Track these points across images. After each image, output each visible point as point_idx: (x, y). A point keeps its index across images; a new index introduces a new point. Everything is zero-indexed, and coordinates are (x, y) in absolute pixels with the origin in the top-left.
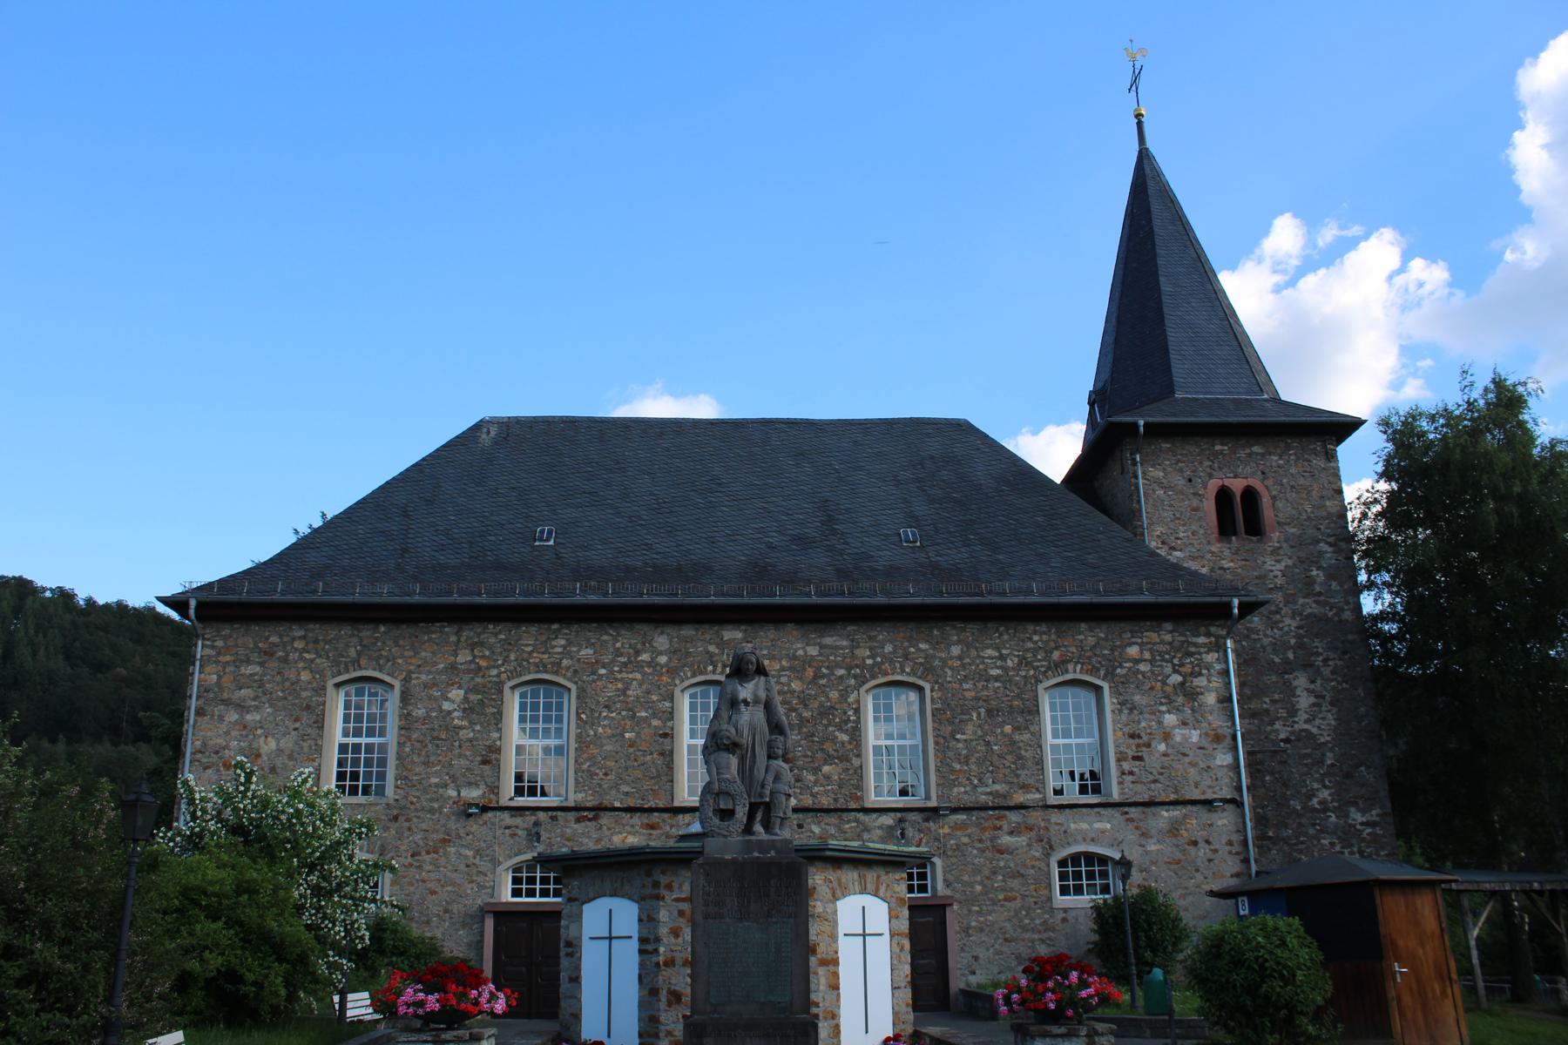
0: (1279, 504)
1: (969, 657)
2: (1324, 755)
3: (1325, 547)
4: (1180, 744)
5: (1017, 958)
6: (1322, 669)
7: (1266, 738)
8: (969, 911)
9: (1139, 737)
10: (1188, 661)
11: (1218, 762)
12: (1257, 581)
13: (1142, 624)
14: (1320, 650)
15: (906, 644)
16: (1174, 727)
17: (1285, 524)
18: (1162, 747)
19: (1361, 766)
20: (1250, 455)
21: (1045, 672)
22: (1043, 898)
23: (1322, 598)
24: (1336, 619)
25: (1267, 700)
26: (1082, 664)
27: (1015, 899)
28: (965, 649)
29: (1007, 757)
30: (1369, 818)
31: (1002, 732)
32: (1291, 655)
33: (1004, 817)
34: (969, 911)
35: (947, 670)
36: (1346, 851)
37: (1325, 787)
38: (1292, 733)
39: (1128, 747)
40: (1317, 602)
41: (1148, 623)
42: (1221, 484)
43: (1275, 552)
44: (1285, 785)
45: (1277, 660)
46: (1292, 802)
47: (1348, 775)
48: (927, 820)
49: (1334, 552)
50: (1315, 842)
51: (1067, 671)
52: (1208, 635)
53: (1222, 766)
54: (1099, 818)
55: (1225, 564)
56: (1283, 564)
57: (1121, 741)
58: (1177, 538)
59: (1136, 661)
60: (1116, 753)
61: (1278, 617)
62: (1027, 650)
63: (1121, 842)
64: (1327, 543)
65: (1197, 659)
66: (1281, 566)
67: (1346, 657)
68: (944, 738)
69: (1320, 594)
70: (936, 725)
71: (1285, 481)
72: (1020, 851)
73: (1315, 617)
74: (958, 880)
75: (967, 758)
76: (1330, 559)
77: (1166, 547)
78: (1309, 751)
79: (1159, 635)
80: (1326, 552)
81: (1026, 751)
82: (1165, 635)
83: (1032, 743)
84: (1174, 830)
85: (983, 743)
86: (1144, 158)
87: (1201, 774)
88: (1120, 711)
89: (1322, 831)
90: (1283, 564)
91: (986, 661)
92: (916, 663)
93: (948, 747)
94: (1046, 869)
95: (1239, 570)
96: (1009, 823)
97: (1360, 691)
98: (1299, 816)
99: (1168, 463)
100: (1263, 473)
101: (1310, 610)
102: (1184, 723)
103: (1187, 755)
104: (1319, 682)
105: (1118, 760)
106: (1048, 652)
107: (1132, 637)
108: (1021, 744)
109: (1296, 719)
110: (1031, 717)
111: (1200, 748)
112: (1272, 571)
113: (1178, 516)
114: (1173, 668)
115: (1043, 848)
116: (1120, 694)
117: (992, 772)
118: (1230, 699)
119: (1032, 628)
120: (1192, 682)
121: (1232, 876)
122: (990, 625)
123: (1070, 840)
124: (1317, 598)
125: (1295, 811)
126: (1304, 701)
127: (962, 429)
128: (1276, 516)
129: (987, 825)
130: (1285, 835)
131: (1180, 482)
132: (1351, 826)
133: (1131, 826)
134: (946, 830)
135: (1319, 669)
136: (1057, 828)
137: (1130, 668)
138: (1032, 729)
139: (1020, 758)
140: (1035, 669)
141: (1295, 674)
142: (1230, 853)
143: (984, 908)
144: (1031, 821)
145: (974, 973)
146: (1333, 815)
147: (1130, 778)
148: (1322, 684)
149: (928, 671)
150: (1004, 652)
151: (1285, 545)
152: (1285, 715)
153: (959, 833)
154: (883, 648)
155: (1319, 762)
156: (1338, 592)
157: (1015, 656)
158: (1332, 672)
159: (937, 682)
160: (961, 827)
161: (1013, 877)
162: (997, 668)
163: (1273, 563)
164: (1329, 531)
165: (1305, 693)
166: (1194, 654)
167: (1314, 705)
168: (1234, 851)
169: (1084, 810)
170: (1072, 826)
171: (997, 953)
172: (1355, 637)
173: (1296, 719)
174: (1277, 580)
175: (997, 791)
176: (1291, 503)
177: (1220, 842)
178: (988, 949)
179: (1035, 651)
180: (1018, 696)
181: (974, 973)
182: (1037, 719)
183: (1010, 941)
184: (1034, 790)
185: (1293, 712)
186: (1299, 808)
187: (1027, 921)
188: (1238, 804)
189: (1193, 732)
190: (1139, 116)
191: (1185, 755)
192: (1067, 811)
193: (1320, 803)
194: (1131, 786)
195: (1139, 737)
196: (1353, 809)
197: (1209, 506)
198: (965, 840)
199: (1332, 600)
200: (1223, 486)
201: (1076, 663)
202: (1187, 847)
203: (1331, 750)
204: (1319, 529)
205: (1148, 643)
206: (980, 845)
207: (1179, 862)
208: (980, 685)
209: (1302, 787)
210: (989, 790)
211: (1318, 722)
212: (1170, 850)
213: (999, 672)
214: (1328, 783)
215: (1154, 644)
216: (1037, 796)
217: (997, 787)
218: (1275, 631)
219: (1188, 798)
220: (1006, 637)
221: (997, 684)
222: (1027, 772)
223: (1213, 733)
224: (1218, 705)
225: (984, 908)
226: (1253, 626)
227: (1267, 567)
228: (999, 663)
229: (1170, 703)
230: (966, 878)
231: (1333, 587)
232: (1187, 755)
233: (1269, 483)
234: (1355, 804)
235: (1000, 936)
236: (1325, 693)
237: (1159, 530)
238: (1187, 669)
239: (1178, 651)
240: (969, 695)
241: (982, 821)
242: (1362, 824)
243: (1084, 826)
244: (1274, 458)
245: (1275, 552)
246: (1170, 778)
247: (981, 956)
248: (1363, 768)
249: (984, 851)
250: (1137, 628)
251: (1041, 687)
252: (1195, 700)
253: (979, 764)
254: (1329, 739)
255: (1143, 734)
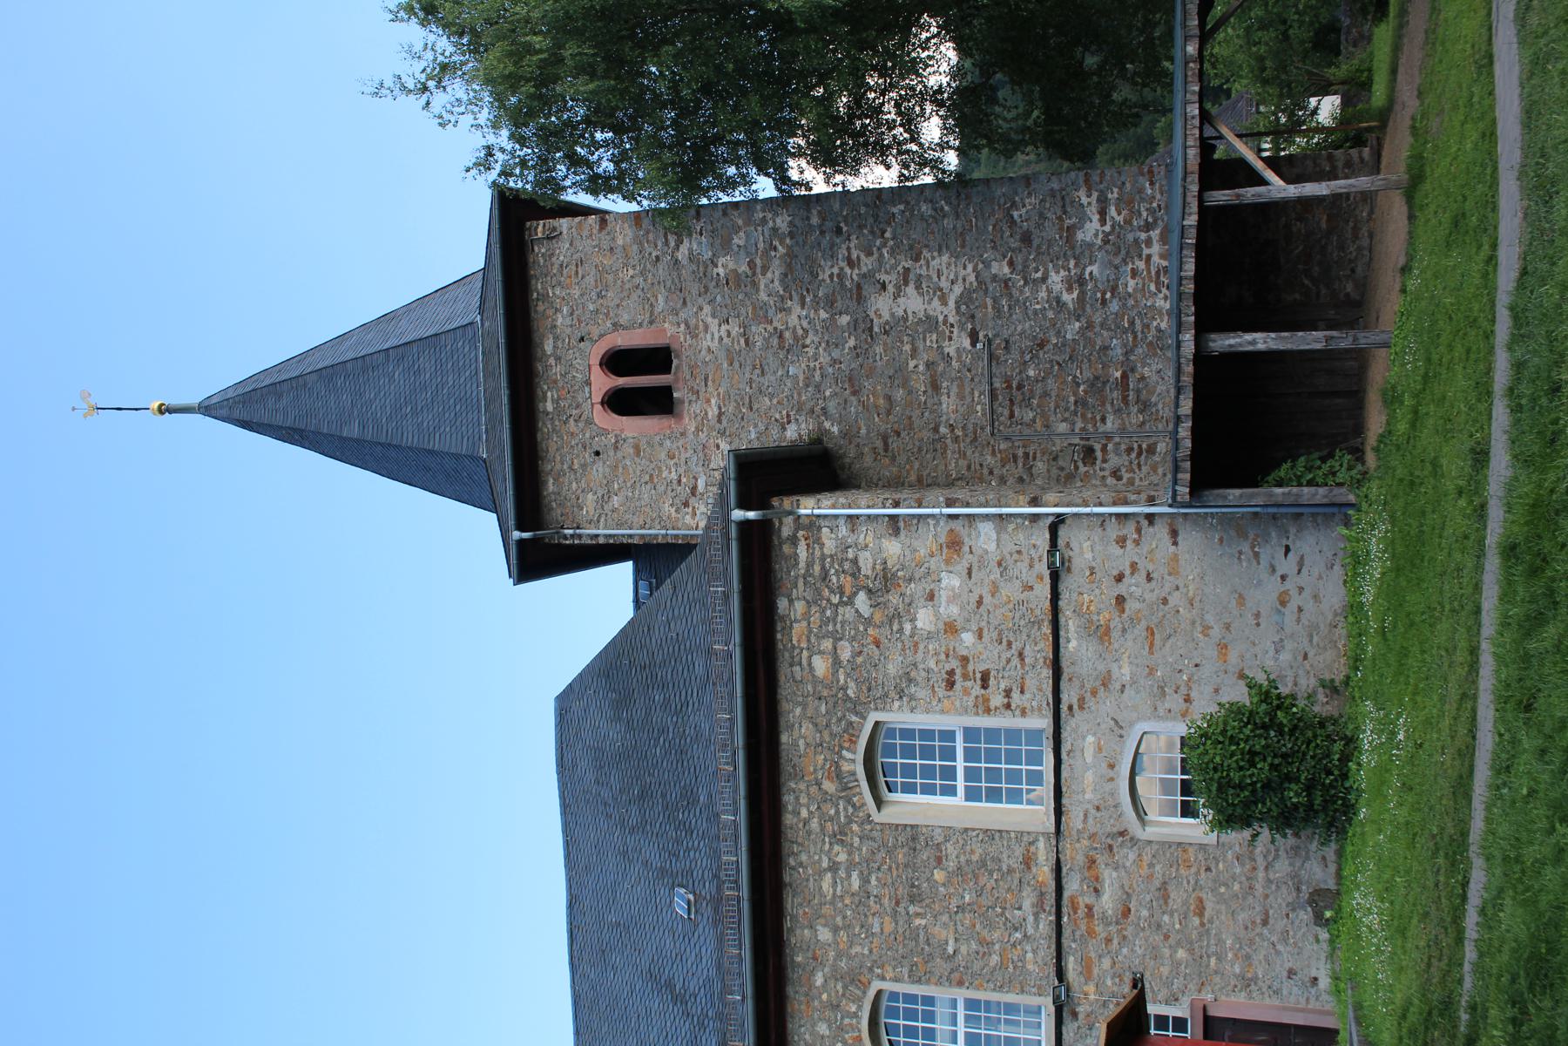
0: (625, 318)
1: (834, 918)
2: (995, 278)
3: (684, 249)
4: (962, 608)
5: (1294, 910)
6: (864, 269)
7: (969, 370)
8: (1216, 972)
9: (951, 673)
10: (834, 579)
11: (992, 547)
12: (736, 364)
13: (780, 646)
14: (836, 271)
15: (816, 1003)
16: (937, 615)
17: (652, 313)
18: (968, 638)
19: (1012, 217)
20: (558, 359)
21: (854, 806)
22: (1200, 857)
23: (758, 261)
24: (788, 241)
25: (912, 364)
26: (842, 748)
27: (1201, 900)
28: (822, 921)
29: (981, 883)
30: (1094, 210)
31: (944, 885)
32: (844, 320)
33: (1072, 899)
34: (1216, 972)
35: (853, 951)
36: (1146, 251)
37: (1044, 279)
38: (962, 327)
39: (966, 692)
40: (765, 269)
41: (779, 636)
42: (600, 406)
43: (692, 332)
44: (1041, 345)
45: (852, 342)
46: (1069, 336)
47: (1026, 239)
48: (1075, 1015)
49: (690, 235)
50: (1131, 302)
51: (853, 774)
52: (794, 540)
53: (998, 540)
54: (1078, 753)
55: (713, 412)
56: (709, 320)
57: (958, 703)
58: (679, 482)
59: (837, 663)
60: (977, 714)
61: (787, 335)
62: (823, 828)
63: (1116, 722)
64: (677, 247)
65: (832, 566)
66: (713, 323)
67: (845, 229)
68: (952, 971)
69: (752, 264)
70: (934, 980)
71: (591, 307)
72: (1126, 883)
73: (786, 275)
74: (1169, 984)
75: (982, 942)
76: (700, 243)
77: (692, 501)
78: (989, 301)
79: (796, 621)
80: (691, 250)
81: (972, 852)
82: (794, 609)
83: (961, 842)
84: (1102, 634)
85: (960, 915)
86: (207, 409)
87: (1010, 580)
88: (912, 698)
89: (1114, 290)
90: (709, 320)
91: (839, 892)
92: (843, 995)
93: (966, 968)
94: (1155, 847)
95: (721, 390)
96: (1083, 893)
97: (895, 210)
98: (1090, 325)
99: (574, 485)
100: (582, 339)
101: (777, 283)
102: (931, 597)
103: (981, 597)
104: (883, 277)
105: (988, 711)
106: (826, 797)
107: (800, 664)
108: (962, 859)
109: (941, 318)
110: (922, 838)
111: (970, 574)
112: (721, 339)
113: (647, 477)
114: (846, 604)
115: (1122, 845)
116: (886, 695)
117: (1004, 909)
118: (893, 518)
119: (789, 816)
120: (867, 577)
121: (1175, 543)
122: (787, 879)
123: (1111, 802)
124: (758, 270)
125: (1082, 330)
126: (913, 303)
127: (566, 704)
128: (641, 325)
129: (1083, 927)
130: (1119, 351)
131: (600, 469)
132: (1106, 242)
133: (1091, 702)
134: (1091, 988)
135: (864, 276)
136: (1090, 820)
137: (848, 675)
138: (941, 839)
139: (983, 863)
140: (850, 821)
141: (872, 315)
142: (1137, 543)
143: (1213, 949)
144: (1081, 859)
145: (1316, 979)
146: (1088, 269)
147: (1016, 695)
148: (887, 273)
149: (855, 979)
150: (825, 864)
151: (682, 315)
152: (934, 337)
153: (1096, 971)
154: (823, 1037)
155: (1006, 285)
156: (748, 236)
157: (831, 849)
158: (869, 254)
159: (871, 969)
160: (1087, 971)
161: (1166, 898)
162: (849, 876)
163: (709, 336)
164: (660, 244)
165: (901, 300)
166: (823, 567)
167: (918, 287)
168: (1135, 536)
169: (1064, 774)
170: (1088, 796)
171: (1285, 939)
172: (815, 212)
173: (941, 318)
174: (734, 333)
175: (1033, 905)
176: (622, 300)
177: (1120, 559)
178: (1278, 953)
179: (824, 819)
180: (890, 852)
181: (1316, 979)
182: (924, 830)
183: (1267, 914)
184: (1032, 849)
185: (930, 323)
186: (1077, 325)
187: (1236, 887)
188: (1059, 520)
189: (944, 583)
190: (163, 410)
191: (980, 603)
192: (1064, 801)
193: (1070, 290)
194: (1028, 695)
195: (951, 673)
196: (1080, 236)
197: (632, 426)
198: (1106, 963)
199: (761, 245)
200: (602, 403)
201: (841, 757)
202: (1125, 615)
203: (987, 265)
204: (657, 258)
205: (809, 641)
206: (1115, 942)
207: (1150, 631)
208: (875, 907)
209: (1045, 317)
210: (1031, 918)
211: (944, 284)
212: (1130, 643)
213: (855, 875)
214: (1039, 275)
215: (810, 631)
216: (1041, 844)
217: (1027, 904)
218: (808, 341)
219: (1048, 603)
220: (804, 857)
221: (874, 882)
222: (1005, 856)
223: (945, 550)
224: (903, 533)
225: (1213, 949)
226: (801, 377)
227: (715, 345)
228: (842, 873)
229: (900, 616)
230: (1165, 970)
231: (741, 243)
232: (981, 597)
233: (595, 332)
234: (1071, 230)
235: (1258, 930)
236: (899, 268)
237: (668, 509)
238: (847, 581)
239: (818, 592)
240: (889, 926)
241: (1078, 933)
242: (1103, 222)
243: (1089, 777)
244: (560, 320)
245: (692, 332)
246: (1017, 630)
247: (1288, 965)
248: (1016, 214)
249: (1124, 937)
250: (787, 655)
251: (877, 817)
252: (894, 575)
253: (991, 926)
254: (970, 267)
255: (948, 667)
